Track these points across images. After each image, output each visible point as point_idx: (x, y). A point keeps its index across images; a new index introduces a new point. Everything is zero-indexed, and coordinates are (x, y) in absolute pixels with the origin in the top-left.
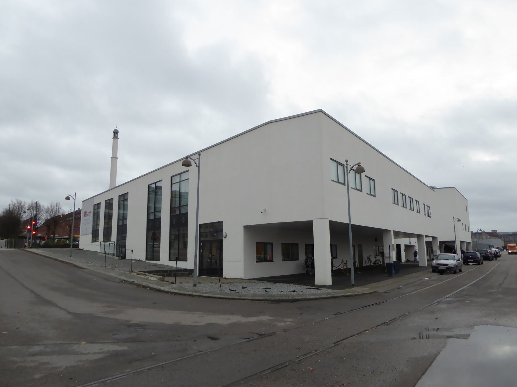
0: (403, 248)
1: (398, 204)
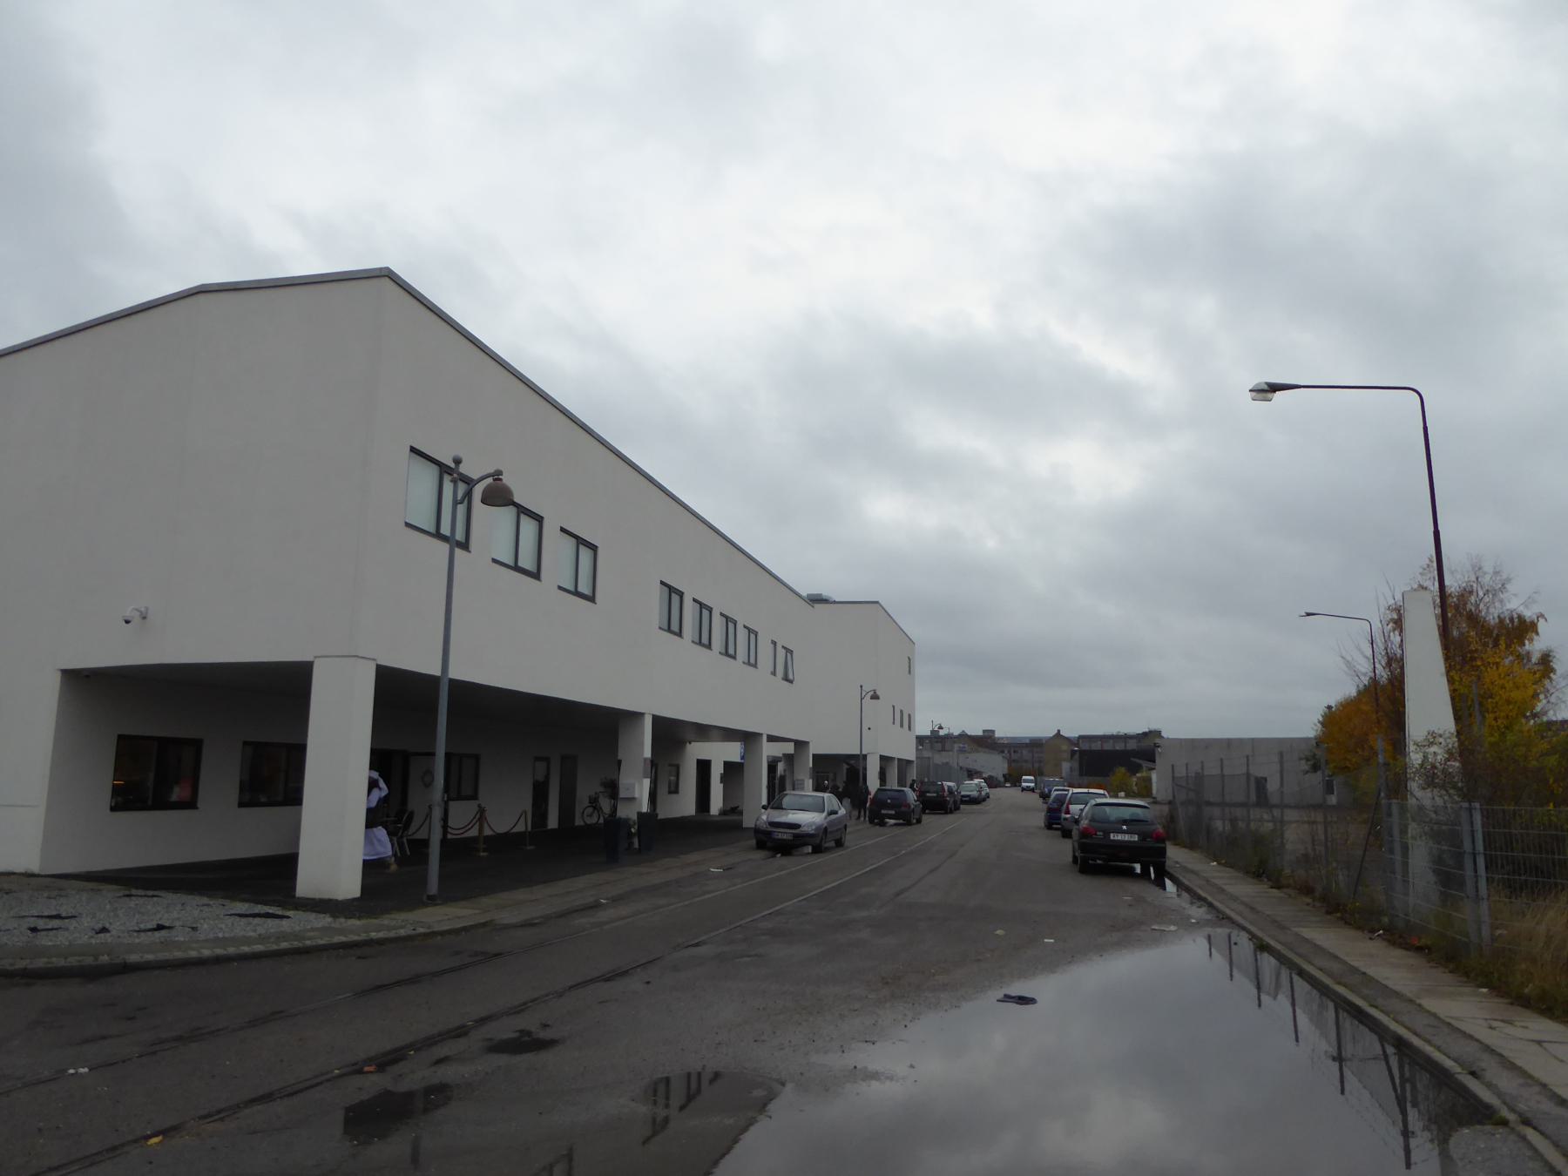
0: (717, 771)
1: (680, 634)
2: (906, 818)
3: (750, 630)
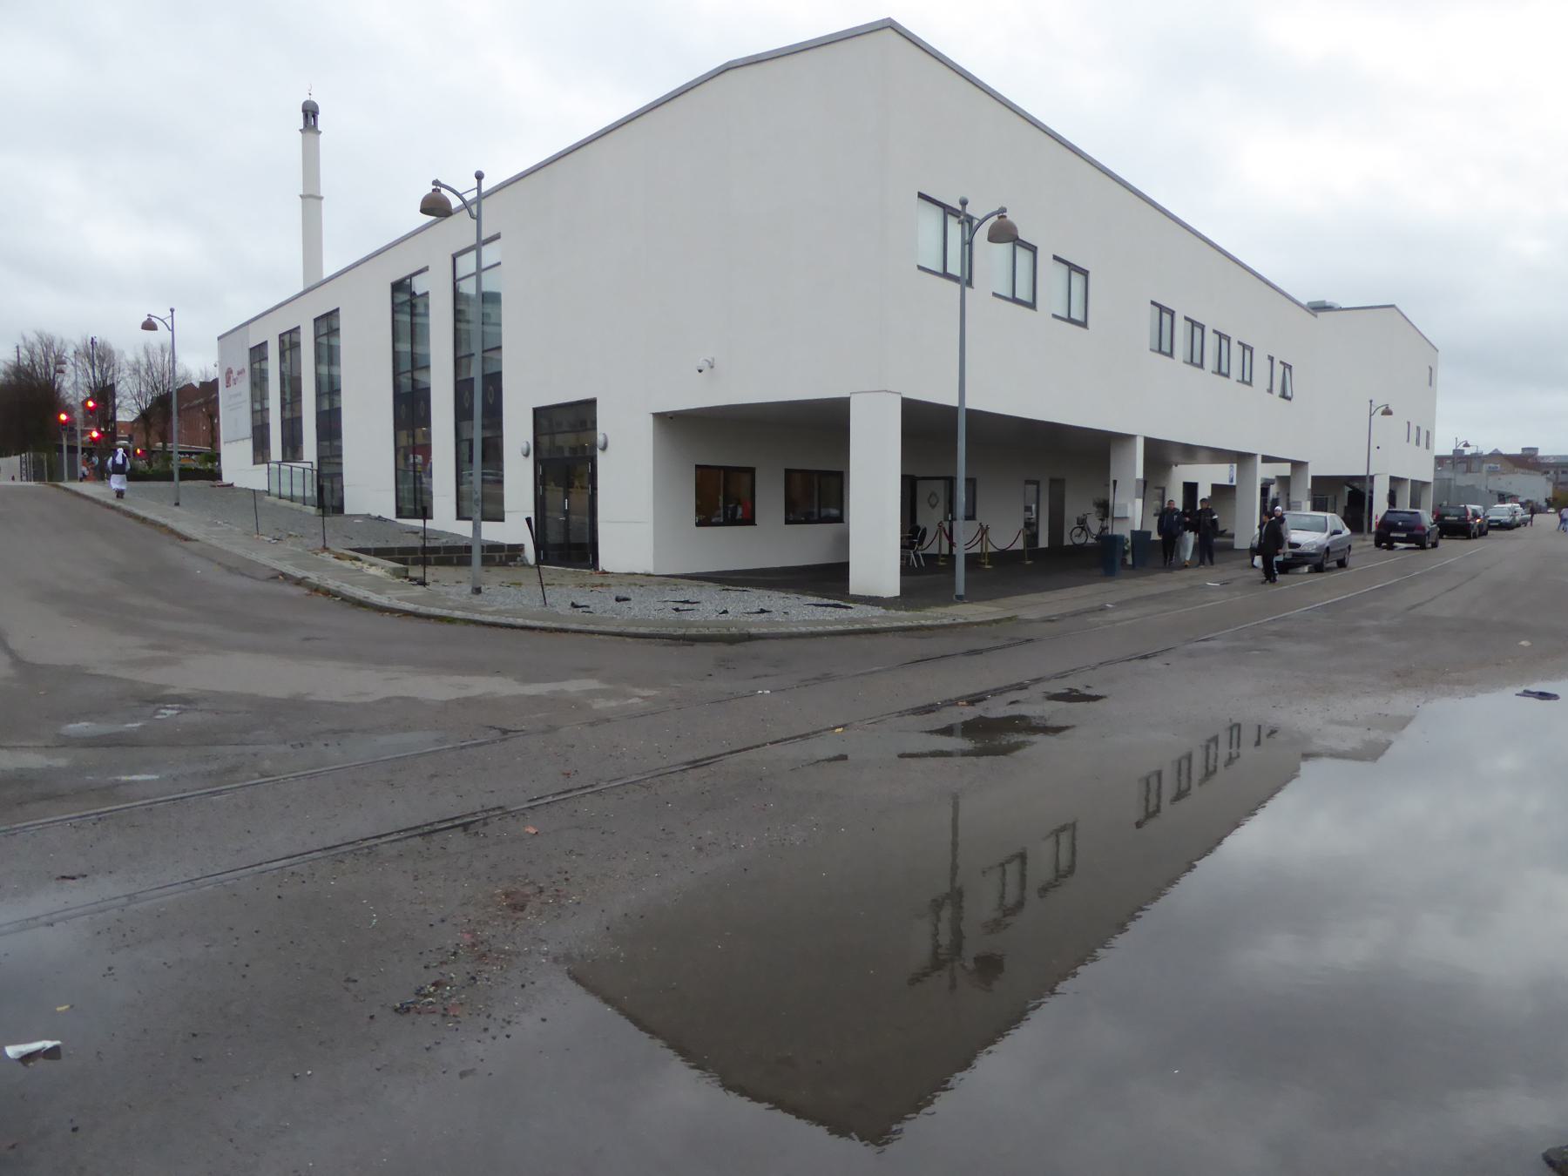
2: (1418, 539)
3: (1244, 346)
